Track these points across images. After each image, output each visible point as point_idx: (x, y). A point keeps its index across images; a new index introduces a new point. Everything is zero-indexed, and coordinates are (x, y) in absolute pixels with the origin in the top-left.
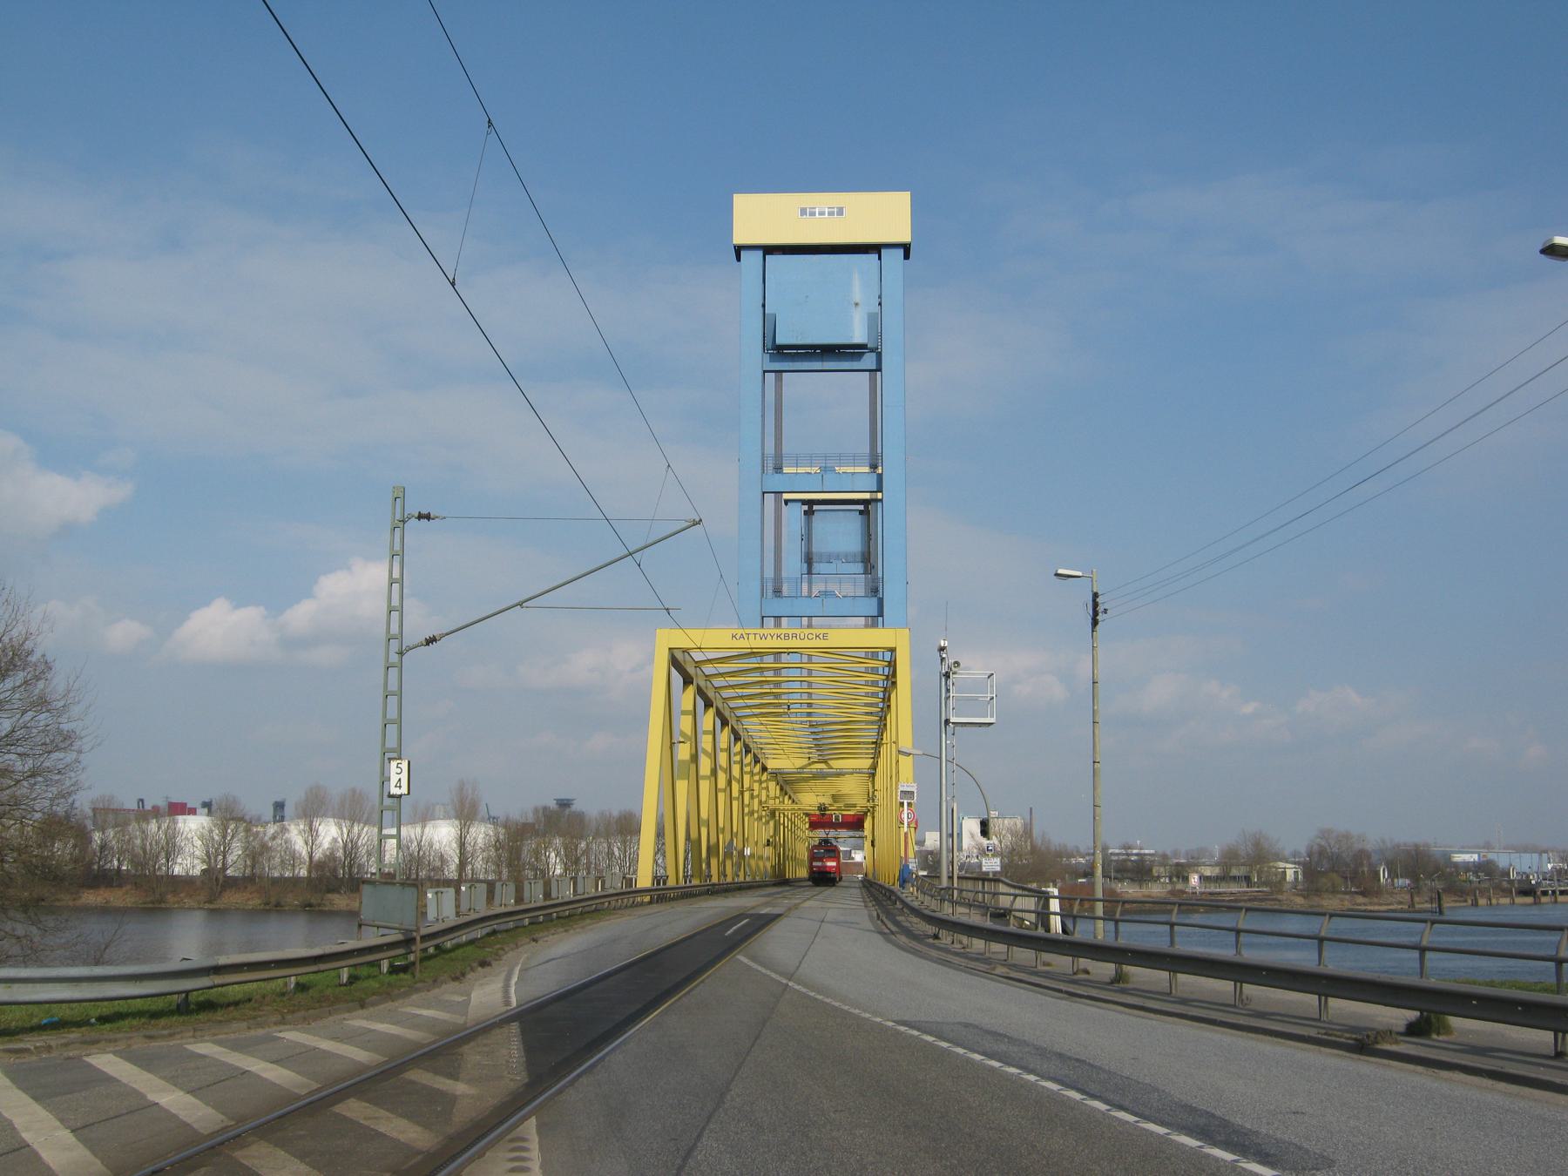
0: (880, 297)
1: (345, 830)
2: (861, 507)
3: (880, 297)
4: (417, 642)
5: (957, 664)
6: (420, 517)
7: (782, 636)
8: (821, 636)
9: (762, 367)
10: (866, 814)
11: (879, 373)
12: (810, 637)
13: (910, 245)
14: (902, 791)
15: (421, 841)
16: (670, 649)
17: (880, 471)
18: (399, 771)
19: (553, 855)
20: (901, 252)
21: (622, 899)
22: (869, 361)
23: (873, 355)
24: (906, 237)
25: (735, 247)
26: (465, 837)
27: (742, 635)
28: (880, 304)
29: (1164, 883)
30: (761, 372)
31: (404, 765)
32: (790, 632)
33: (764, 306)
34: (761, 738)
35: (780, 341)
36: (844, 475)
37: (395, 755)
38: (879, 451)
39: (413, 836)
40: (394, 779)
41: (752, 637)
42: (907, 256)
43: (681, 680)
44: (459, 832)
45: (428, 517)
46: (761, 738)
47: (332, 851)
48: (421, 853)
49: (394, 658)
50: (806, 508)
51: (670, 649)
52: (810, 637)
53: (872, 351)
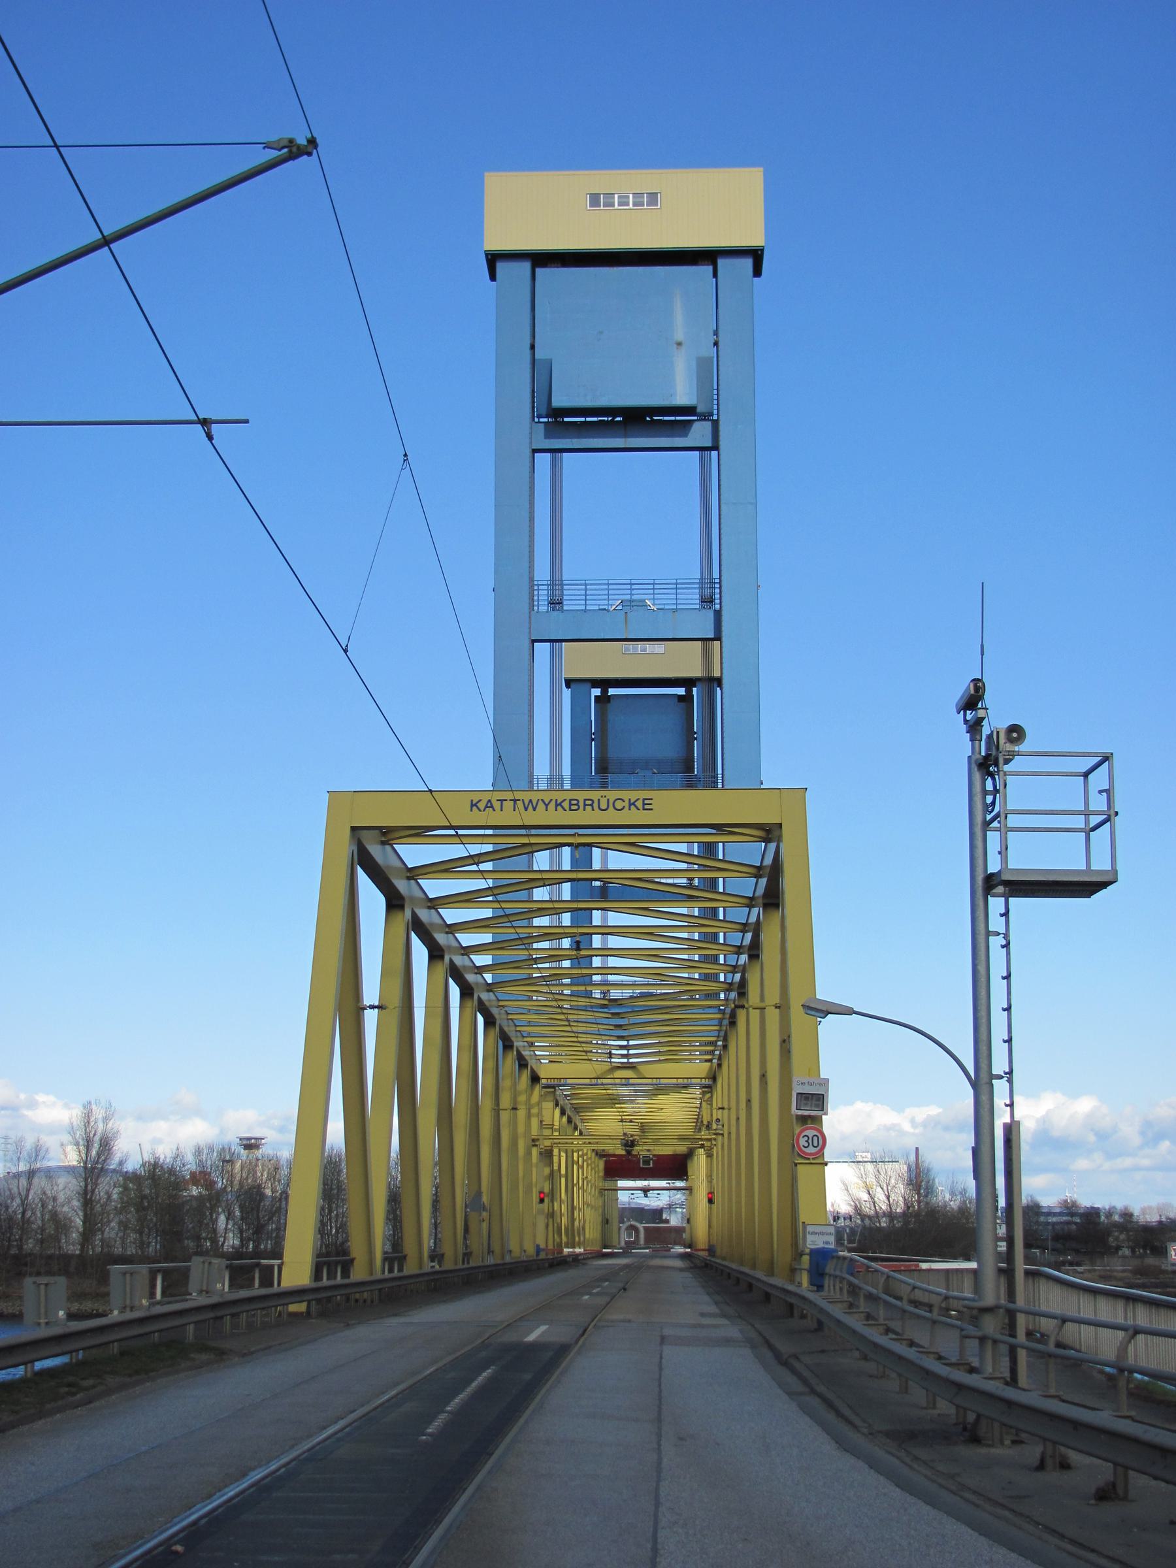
0: (716, 333)
2: (681, 691)
3: (716, 333)
5: (1016, 733)
7: (566, 805)
9: (531, 443)
10: (690, 1154)
11: (714, 453)
12: (619, 805)
13: (762, 250)
14: (798, 1094)
15: (27, 1196)
16: (354, 829)
17: (717, 607)
19: (222, 1218)
20: (748, 263)
21: (233, 1315)
22: (700, 433)
23: (707, 425)
24: (755, 240)
25: (487, 255)
26: (93, 1191)
28: (716, 344)
29: (1124, 1257)
30: (528, 452)
32: (581, 796)
33: (533, 347)
34: (529, 1024)
35: (559, 401)
36: (661, 612)
38: (716, 575)
39: (15, 1190)
42: (757, 272)
43: (380, 900)
44: (83, 1184)
46: (529, 1024)
47: (908, 1206)
48: (29, 1214)
50: (597, 692)
51: (354, 829)
52: (619, 805)
53: (705, 417)
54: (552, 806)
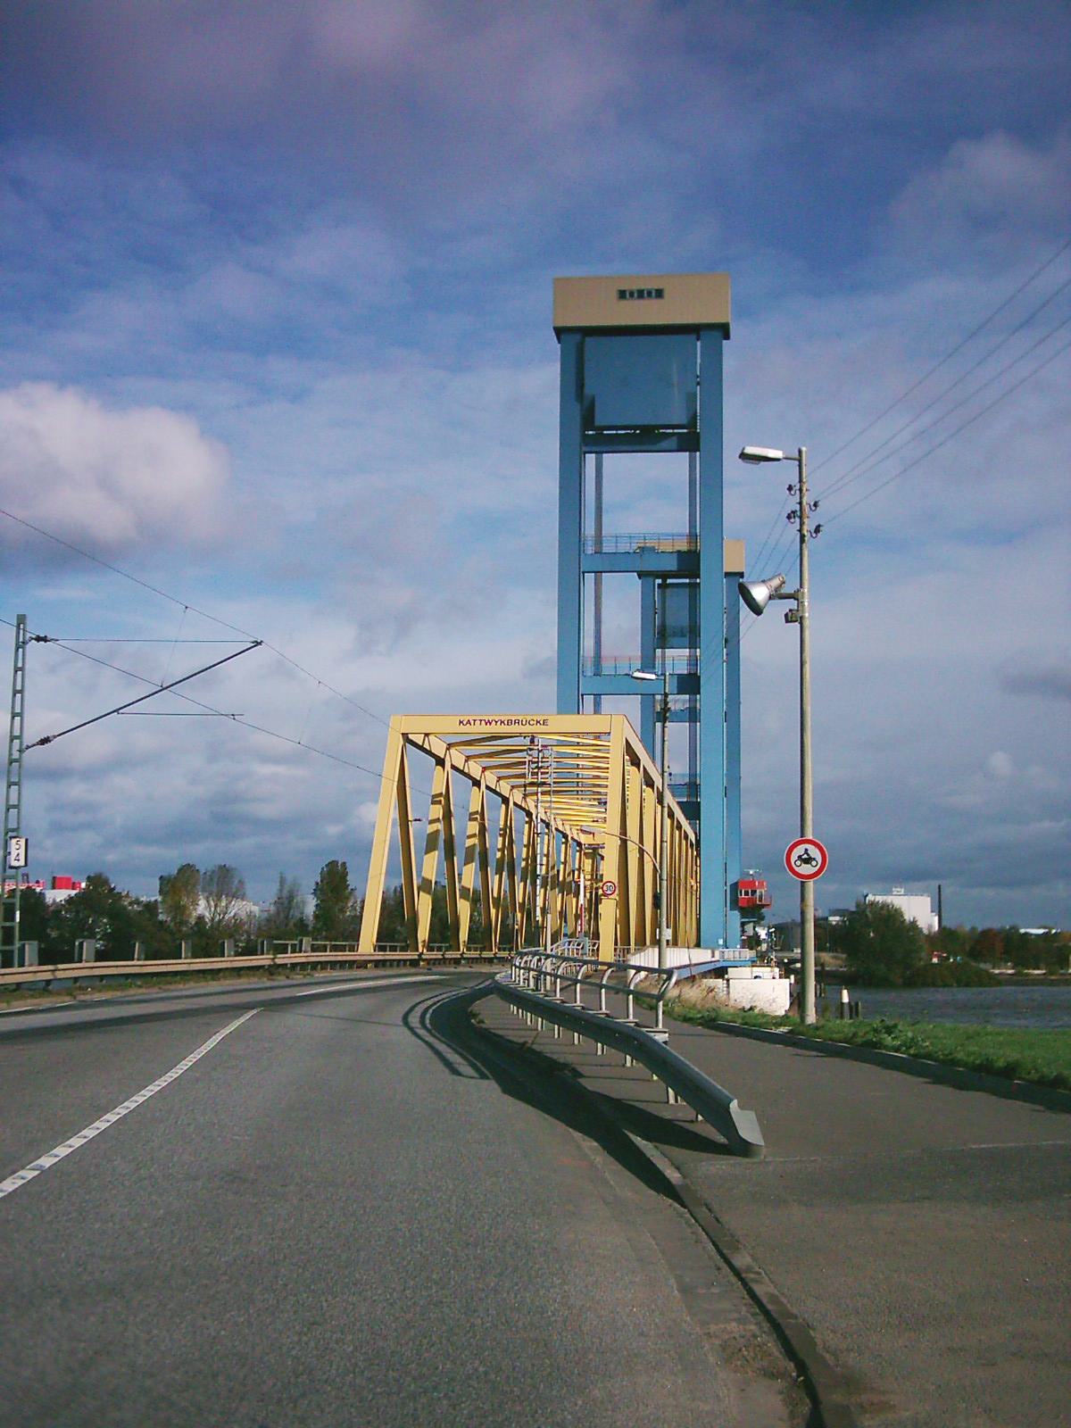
1: (212, 903)
4: (35, 742)
6: (38, 639)
8: (542, 722)
18: (18, 847)
27: (469, 722)
31: (23, 842)
37: (14, 834)
40: (13, 856)
41: (478, 722)
45: (45, 639)
49: (16, 755)
50: (659, 581)
54: (483, 722)
